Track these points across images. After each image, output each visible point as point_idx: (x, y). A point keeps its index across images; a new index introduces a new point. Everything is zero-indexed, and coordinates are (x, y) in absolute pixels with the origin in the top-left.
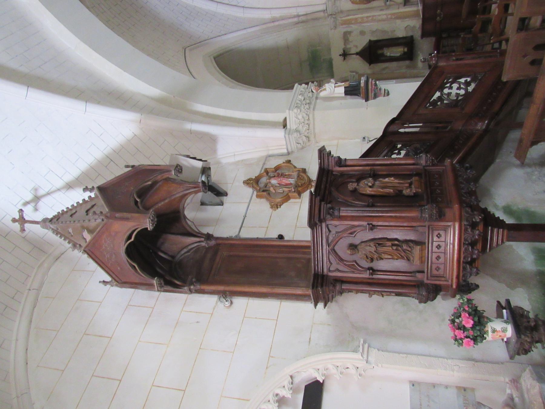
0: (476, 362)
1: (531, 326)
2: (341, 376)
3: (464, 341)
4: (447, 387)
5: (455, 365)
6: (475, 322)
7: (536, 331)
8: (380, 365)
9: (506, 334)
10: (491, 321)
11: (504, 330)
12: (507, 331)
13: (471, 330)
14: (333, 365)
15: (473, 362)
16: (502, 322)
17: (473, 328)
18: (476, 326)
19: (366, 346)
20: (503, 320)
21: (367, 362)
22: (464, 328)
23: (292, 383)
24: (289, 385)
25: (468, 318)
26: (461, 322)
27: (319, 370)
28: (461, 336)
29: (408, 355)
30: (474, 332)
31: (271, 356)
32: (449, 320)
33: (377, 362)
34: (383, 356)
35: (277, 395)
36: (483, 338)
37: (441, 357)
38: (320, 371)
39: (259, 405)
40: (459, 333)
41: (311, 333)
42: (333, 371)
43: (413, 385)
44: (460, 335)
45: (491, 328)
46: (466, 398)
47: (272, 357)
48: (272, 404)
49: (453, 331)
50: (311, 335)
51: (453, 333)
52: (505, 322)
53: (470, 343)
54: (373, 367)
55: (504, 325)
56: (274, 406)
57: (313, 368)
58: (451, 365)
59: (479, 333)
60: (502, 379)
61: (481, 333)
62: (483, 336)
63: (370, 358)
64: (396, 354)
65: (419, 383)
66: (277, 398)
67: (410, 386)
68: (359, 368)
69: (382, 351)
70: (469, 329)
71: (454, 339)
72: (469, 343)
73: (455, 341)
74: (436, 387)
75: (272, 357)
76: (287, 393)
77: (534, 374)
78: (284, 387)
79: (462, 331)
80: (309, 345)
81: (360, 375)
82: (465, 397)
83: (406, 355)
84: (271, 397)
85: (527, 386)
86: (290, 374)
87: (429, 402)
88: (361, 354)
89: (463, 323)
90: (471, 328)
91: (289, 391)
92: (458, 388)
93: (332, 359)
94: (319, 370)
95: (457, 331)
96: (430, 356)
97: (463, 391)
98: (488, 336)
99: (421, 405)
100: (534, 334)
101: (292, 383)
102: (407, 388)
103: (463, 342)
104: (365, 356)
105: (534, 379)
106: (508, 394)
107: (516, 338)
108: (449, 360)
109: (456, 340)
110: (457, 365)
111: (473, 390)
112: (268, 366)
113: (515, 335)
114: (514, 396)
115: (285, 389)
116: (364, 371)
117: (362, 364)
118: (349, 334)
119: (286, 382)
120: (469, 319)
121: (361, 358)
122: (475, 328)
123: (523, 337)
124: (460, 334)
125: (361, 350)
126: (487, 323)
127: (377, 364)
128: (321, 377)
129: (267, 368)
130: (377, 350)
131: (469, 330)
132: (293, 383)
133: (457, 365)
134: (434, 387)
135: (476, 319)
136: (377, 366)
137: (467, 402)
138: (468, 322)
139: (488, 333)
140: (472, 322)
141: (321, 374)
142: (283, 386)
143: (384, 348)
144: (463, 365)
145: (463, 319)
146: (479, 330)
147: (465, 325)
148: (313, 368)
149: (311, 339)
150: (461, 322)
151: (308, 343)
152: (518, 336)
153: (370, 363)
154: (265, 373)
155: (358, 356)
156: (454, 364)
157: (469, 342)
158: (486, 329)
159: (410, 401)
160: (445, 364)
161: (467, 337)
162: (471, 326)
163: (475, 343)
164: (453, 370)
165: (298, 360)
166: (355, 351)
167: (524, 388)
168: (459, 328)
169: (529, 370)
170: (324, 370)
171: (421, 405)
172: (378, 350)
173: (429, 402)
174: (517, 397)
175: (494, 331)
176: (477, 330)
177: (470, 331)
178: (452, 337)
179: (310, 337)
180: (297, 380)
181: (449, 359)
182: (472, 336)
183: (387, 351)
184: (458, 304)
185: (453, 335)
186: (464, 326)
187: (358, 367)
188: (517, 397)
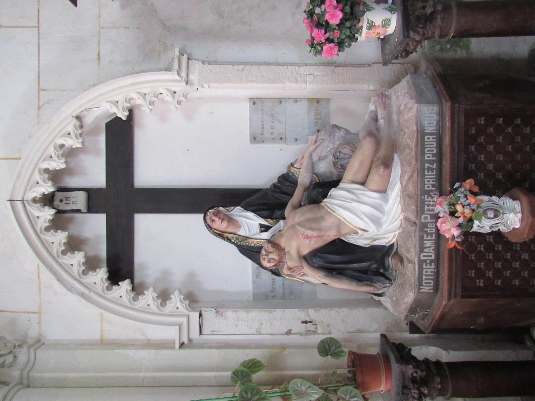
0: (337, 66)
1: (426, 15)
2: (151, 107)
3: (324, 48)
4: (296, 101)
5: (309, 75)
6: (345, 14)
7: (431, 23)
8: (206, 85)
9: (387, 29)
10: (369, 10)
11: (386, 24)
12: (389, 25)
13: (337, 30)
14: (139, 93)
15: (333, 68)
16: (385, 10)
17: (341, 25)
18: (346, 20)
19: (185, 58)
20: (386, 6)
21: (187, 83)
22: (327, 26)
23: (81, 127)
24: (75, 130)
25: (336, 8)
26: (323, 14)
27: (117, 102)
28: (321, 40)
29: (247, 67)
30: (341, 32)
31: (41, 89)
32: (305, 12)
33: (202, 81)
34: (209, 71)
35: (62, 146)
36: (353, 38)
37: (292, 64)
38: (120, 104)
39: (37, 165)
40: (319, 35)
41: (99, 43)
42: (139, 101)
43: (254, 103)
44: (319, 37)
45: (367, 23)
46: (318, 112)
47: (44, 90)
48: (56, 161)
49: (310, 29)
50: (99, 48)
51: (309, 32)
52: (389, 10)
53: (333, 51)
54: (198, 89)
55: (388, 15)
56: (59, 164)
57: (60, 137)
58: (304, 74)
59: (348, 33)
60: (365, 87)
61: (351, 33)
62: (354, 36)
63: (191, 77)
64: (228, 66)
65: (262, 100)
66: (61, 152)
67: (250, 105)
68: (176, 93)
69: (209, 64)
70: (335, 27)
71: (309, 45)
72: (331, 51)
73: (312, 47)
74: (283, 103)
75: (44, 90)
76: (75, 143)
77: (413, 89)
78: (69, 134)
79: (323, 32)
80: (99, 65)
81: (179, 103)
82: (318, 111)
83: (243, 66)
84: (51, 151)
85: (401, 105)
86: (75, 114)
87: (273, 122)
88: (176, 73)
89: (327, 17)
90: (337, 25)
91: (77, 139)
92: (311, 100)
93: (134, 84)
94: (118, 103)
95: (316, 31)
96: (277, 64)
97: (315, 103)
98: (361, 35)
99: (263, 127)
100: (428, 27)
101: (81, 127)
102: (246, 107)
103: (322, 49)
104: (184, 75)
105: (412, 98)
106: (371, 111)
107: (402, 36)
108: (301, 67)
109: (312, 46)
110: (312, 74)
111: (328, 100)
112: (40, 105)
113: (400, 30)
114: (379, 117)
115: (72, 138)
116: (183, 96)
117: (180, 87)
118: (160, 41)
119: (71, 126)
120: (336, 11)
121: (178, 78)
122: (344, 24)
123: (412, 34)
124: (320, 35)
125: (176, 66)
126: (363, 13)
127: (202, 84)
128: (122, 113)
129: (39, 108)
130: (201, 64)
131: (335, 29)
132: (84, 125)
133: (312, 74)
134: (281, 102)
135: (348, 9)
136: (202, 87)
137: (319, 117)
138: (334, 16)
139: (362, 30)
140: (340, 15)
141: (121, 109)
142: (68, 133)
143: (213, 57)
144: (319, 74)
145: (328, 10)
146: (350, 28)
147: (328, 21)
148: (60, 137)
149: (100, 55)
150: (323, 14)
151: (98, 61)
152: (406, 34)
153: (192, 85)
154: (38, 116)
155: (173, 76)
156: (308, 73)
157: (331, 49)
158: (360, 24)
159: (250, 124)
160: (295, 74)
161: (329, 40)
162: (338, 22)
163: (341, 48)
164: (305, 82)
165: (85, 90)
166: (168, 69)
167: (394, 110)
168: (319, 25)
169: (407, 81)
170: (124, 102)
171: (263, 127)
172: (202, 63)
173: (273, 122)
174: (382, 118)
175: (371, 26)
176: (347, 27)
177: (335, 31)
178: (307, 41)
179: (97, 52)
180: (89, 120)
181: (302, 66)
182: (338, 39)
183: (216, 63)
184: (310, 47)
185: (309, 37)
186: (327, 22)
187: (175, 91)
188: (382, 118)
